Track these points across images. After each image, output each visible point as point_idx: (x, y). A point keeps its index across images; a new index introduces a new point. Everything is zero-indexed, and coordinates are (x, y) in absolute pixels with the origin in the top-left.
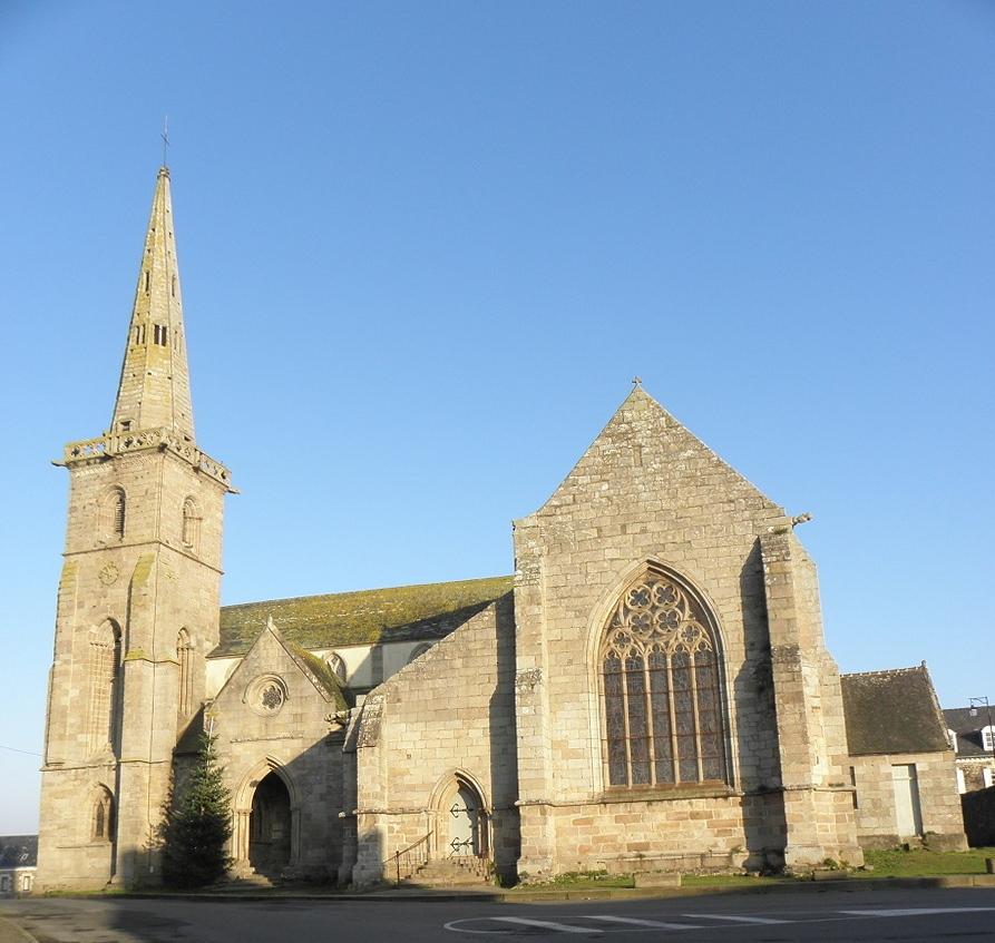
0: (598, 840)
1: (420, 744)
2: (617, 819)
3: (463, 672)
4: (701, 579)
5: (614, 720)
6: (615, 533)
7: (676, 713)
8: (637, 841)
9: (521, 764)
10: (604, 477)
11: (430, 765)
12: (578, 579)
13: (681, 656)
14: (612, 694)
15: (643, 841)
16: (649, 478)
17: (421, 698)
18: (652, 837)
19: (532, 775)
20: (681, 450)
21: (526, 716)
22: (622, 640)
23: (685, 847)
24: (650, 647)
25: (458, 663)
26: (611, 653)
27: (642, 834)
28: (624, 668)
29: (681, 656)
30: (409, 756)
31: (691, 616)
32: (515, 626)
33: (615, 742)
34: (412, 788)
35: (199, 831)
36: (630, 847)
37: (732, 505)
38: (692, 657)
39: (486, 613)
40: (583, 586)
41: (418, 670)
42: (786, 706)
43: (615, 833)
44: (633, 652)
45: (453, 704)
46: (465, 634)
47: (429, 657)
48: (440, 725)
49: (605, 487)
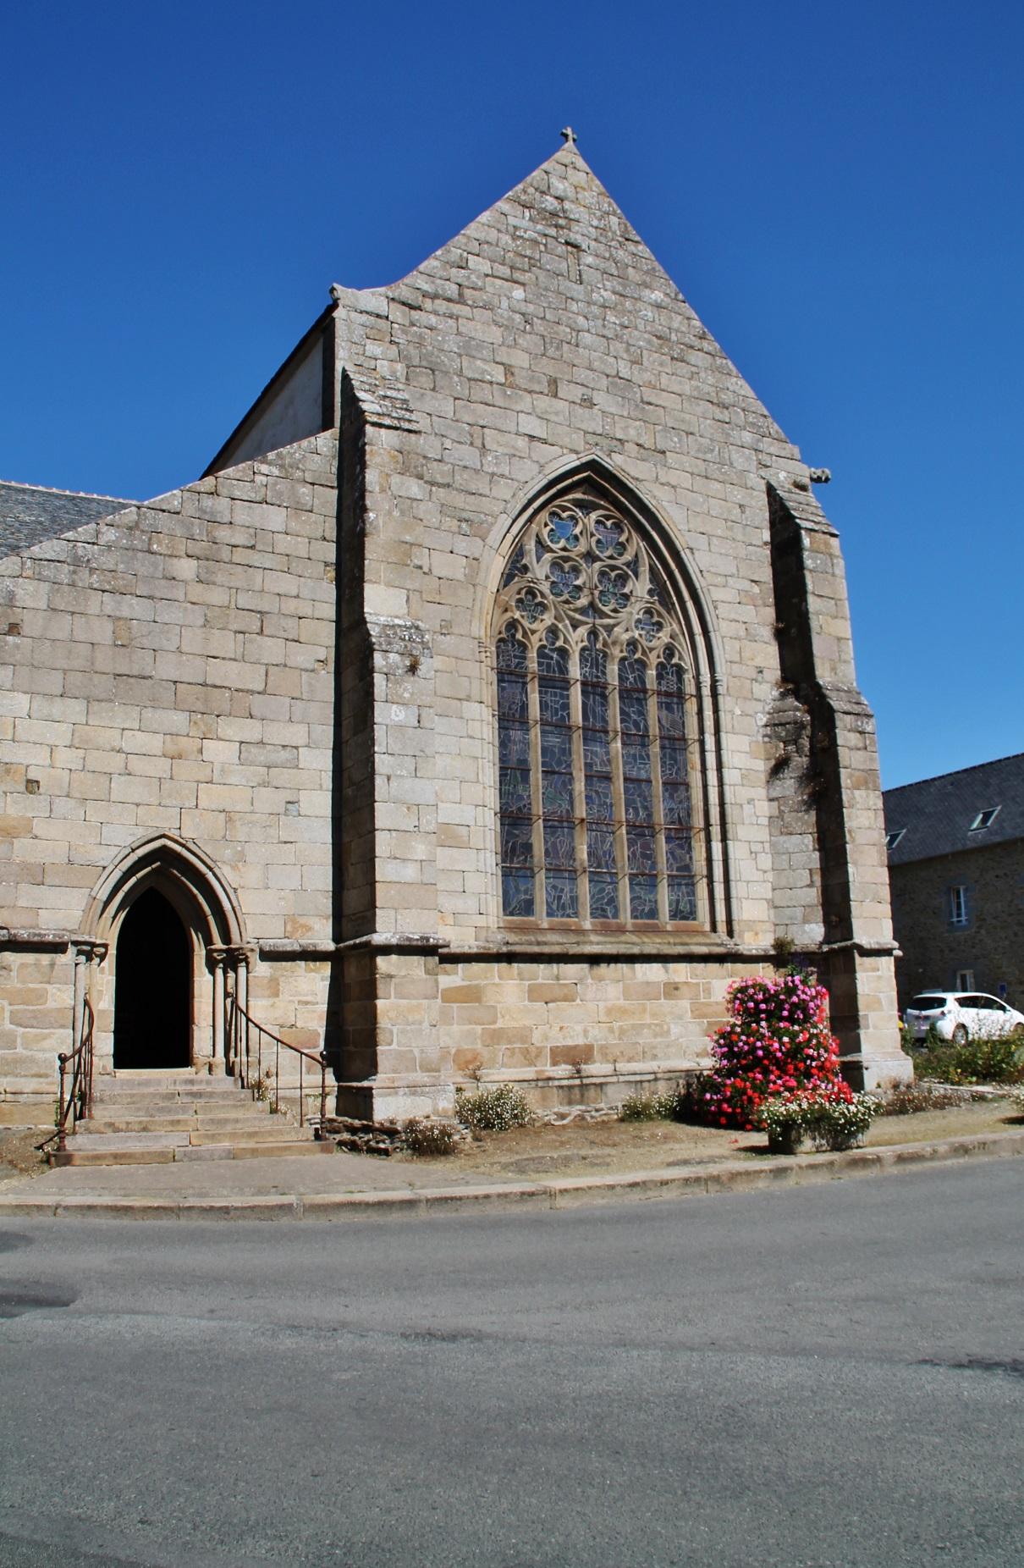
0: (495, 1037)
1: (65, 757)
2: (534, 994)
3: (197, 592)
4: (683, 527)
5: (512, 772)
6: (537, 388)
7: (687, 786)
8: (570, 1043)
9: (383, 844)
10: (517, 275)
11: (93, 818)
12: (469, 455)
13: (633, 665)
14: (510, 718)
15: (581, 1041)
16: (595, 309)
17: (80, 635)
18: (596, 1035)
19: (410, 872)
20: (646, 286)
21: (401, 727)
22: (531, 601)
23: (655, 1057)
24: (582, 631)
25: (186, 568)
26: (512, 625)
27: (579, 1028)
28: (533, 665)
29: (633, 665)
30: (32, 785)
31: (650, 592)
32: (364, 509)
33: (513, 819)
34: (38, 875)
35: (409, 1481)
36: (560, 1055)
37: (726, 412)
38: (652, 673)
39: (264, 468)
40: (476, 471)
41: (77, 562)
42: (857, 792)
43: (528, 1022)
44: (553, 631)
45: (167, 669)
46: (208, 502)
47: (109, 535)
48: (124, 716)
49: (519, 293)
